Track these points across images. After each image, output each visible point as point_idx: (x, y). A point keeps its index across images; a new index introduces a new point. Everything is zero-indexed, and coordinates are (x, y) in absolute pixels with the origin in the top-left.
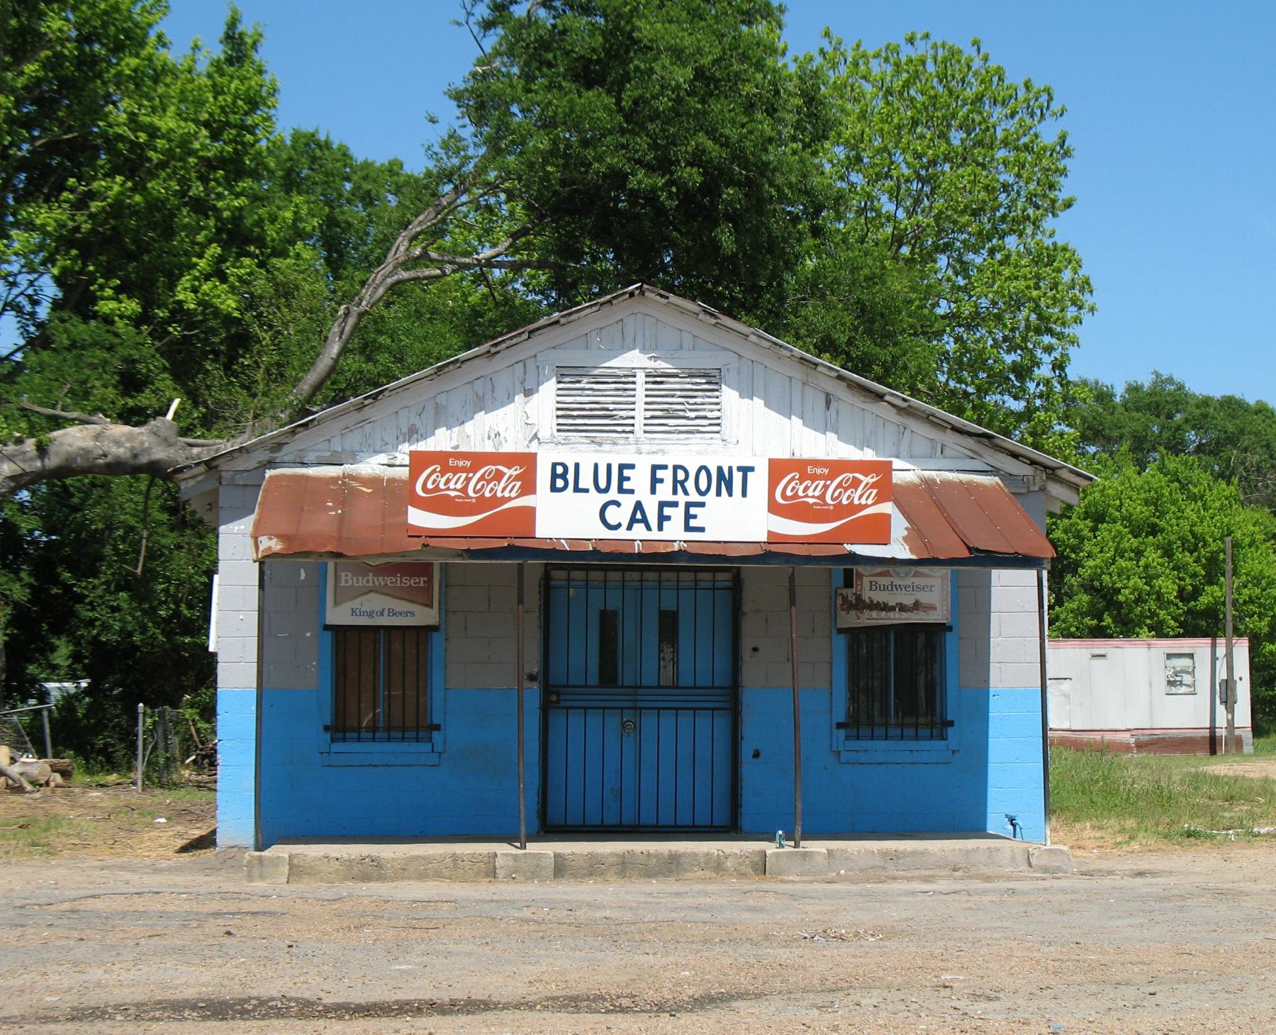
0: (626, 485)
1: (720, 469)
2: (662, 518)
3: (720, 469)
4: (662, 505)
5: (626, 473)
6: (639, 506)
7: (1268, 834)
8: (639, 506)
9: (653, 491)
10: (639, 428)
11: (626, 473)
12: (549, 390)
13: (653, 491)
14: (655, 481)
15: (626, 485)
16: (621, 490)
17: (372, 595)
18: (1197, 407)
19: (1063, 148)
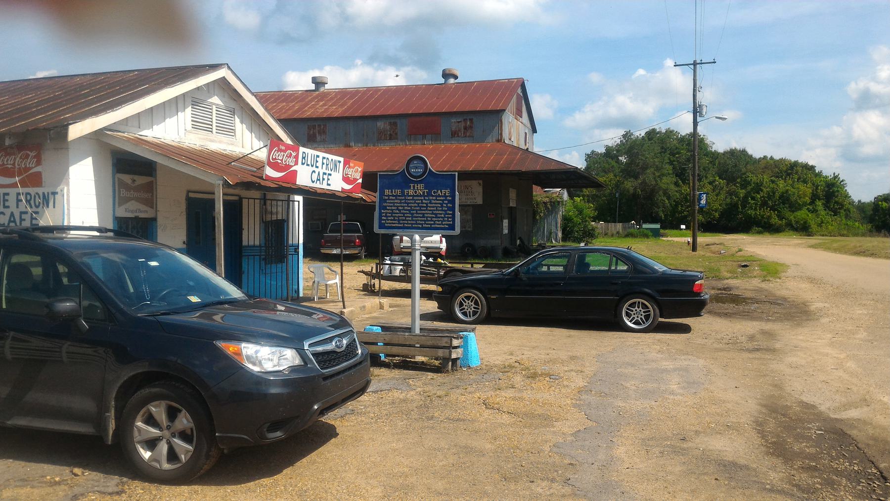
0: (7, 204)
1: (44, 193)
2: (22, 220)
3: (44, 193)
4: (21, 213)
5: (6, 197)
6: (12, 214)
7: (117, 419)
8: (12, 214)
9: (17, 207)
10: (214, 131)
11: (6, 197)
12: (189, 110)
13: (17, 207)
14: (19, 200)
15: (7, 204)
16: (5, 207)
17: (133, 202)
18: (849, 203)
19: (330, 433)
